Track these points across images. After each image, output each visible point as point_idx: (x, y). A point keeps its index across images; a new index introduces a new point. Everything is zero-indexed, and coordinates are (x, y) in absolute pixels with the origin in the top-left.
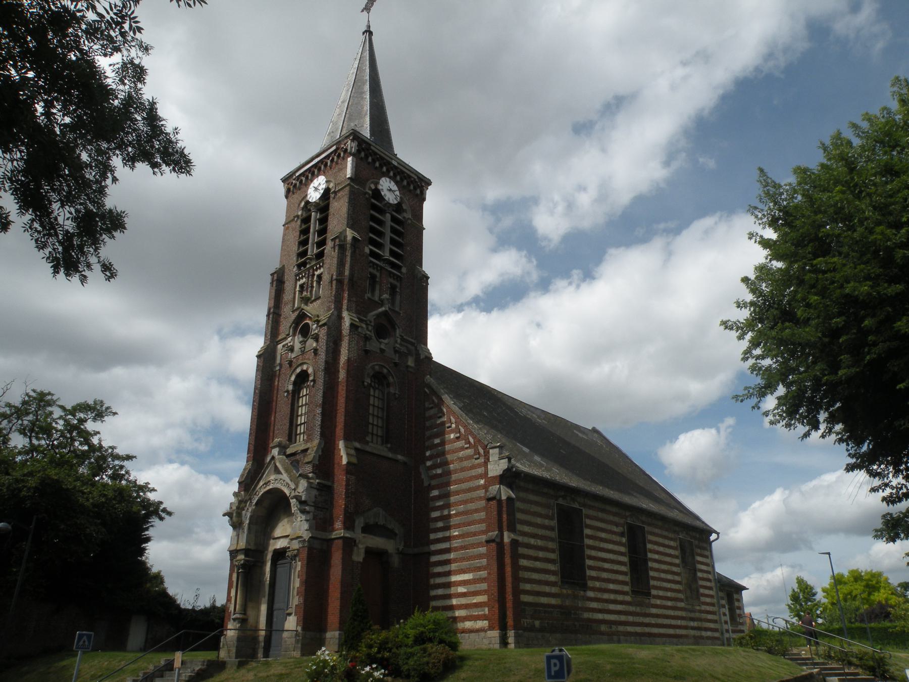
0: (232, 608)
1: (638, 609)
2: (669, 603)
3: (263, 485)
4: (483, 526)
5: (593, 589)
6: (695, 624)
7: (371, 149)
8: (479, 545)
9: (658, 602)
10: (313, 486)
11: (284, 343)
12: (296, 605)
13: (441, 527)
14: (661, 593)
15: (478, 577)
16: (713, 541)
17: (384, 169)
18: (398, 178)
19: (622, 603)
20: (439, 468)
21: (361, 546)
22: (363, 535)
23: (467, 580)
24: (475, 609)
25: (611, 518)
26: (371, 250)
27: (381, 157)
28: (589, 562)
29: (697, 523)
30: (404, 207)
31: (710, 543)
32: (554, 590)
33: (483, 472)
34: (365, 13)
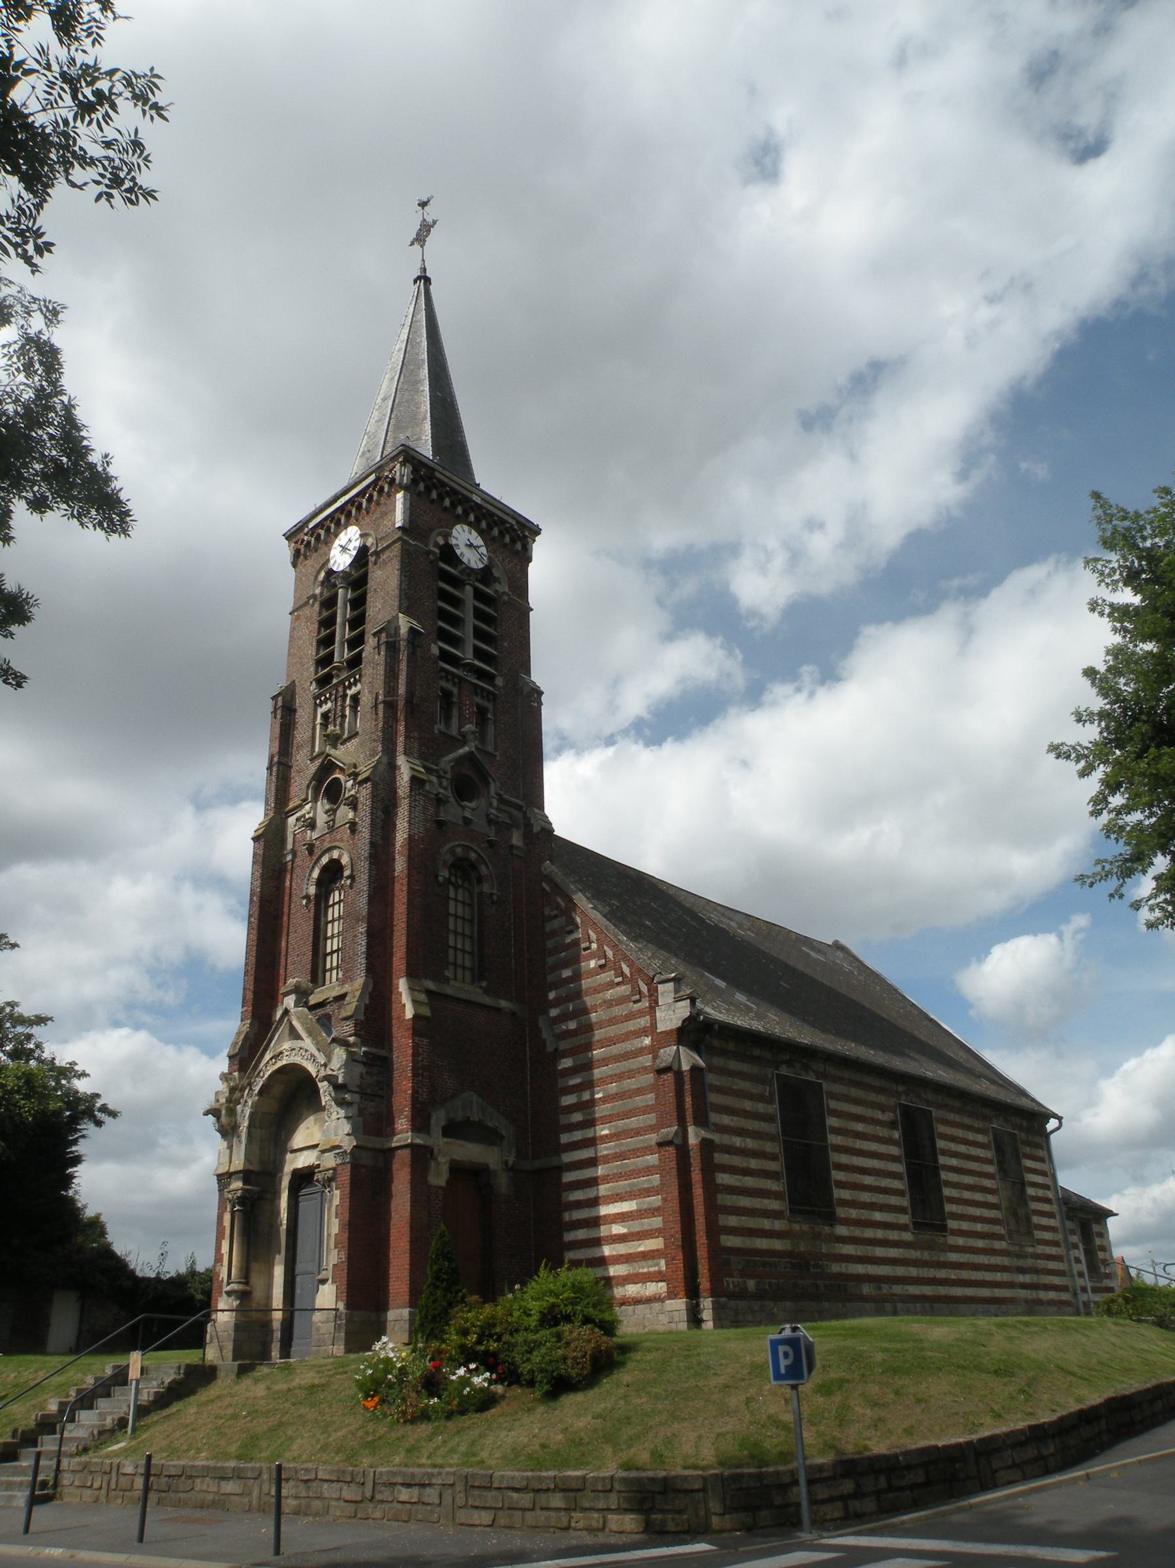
0: (224, 1274)
1: (926, 1256)
2: (980, 1243)
3: (271, 1059)
5: (846, 1222)
8: (646, 1150)
9: (961, 1241)
10: (356, 1057)
14: (965, 1226)
16: (1052, 1132)
17: (460, 510)
18: (484, 524)
21: (441, 1159)
22: (445, 1140)
23: (627, 1212)
25: (872, 1097)
26: (441, 650)
27: (452, 489)
28: (836, 1175)
29: (1024, 1102)
31: (1046, 1136)
32: (778, 1225)
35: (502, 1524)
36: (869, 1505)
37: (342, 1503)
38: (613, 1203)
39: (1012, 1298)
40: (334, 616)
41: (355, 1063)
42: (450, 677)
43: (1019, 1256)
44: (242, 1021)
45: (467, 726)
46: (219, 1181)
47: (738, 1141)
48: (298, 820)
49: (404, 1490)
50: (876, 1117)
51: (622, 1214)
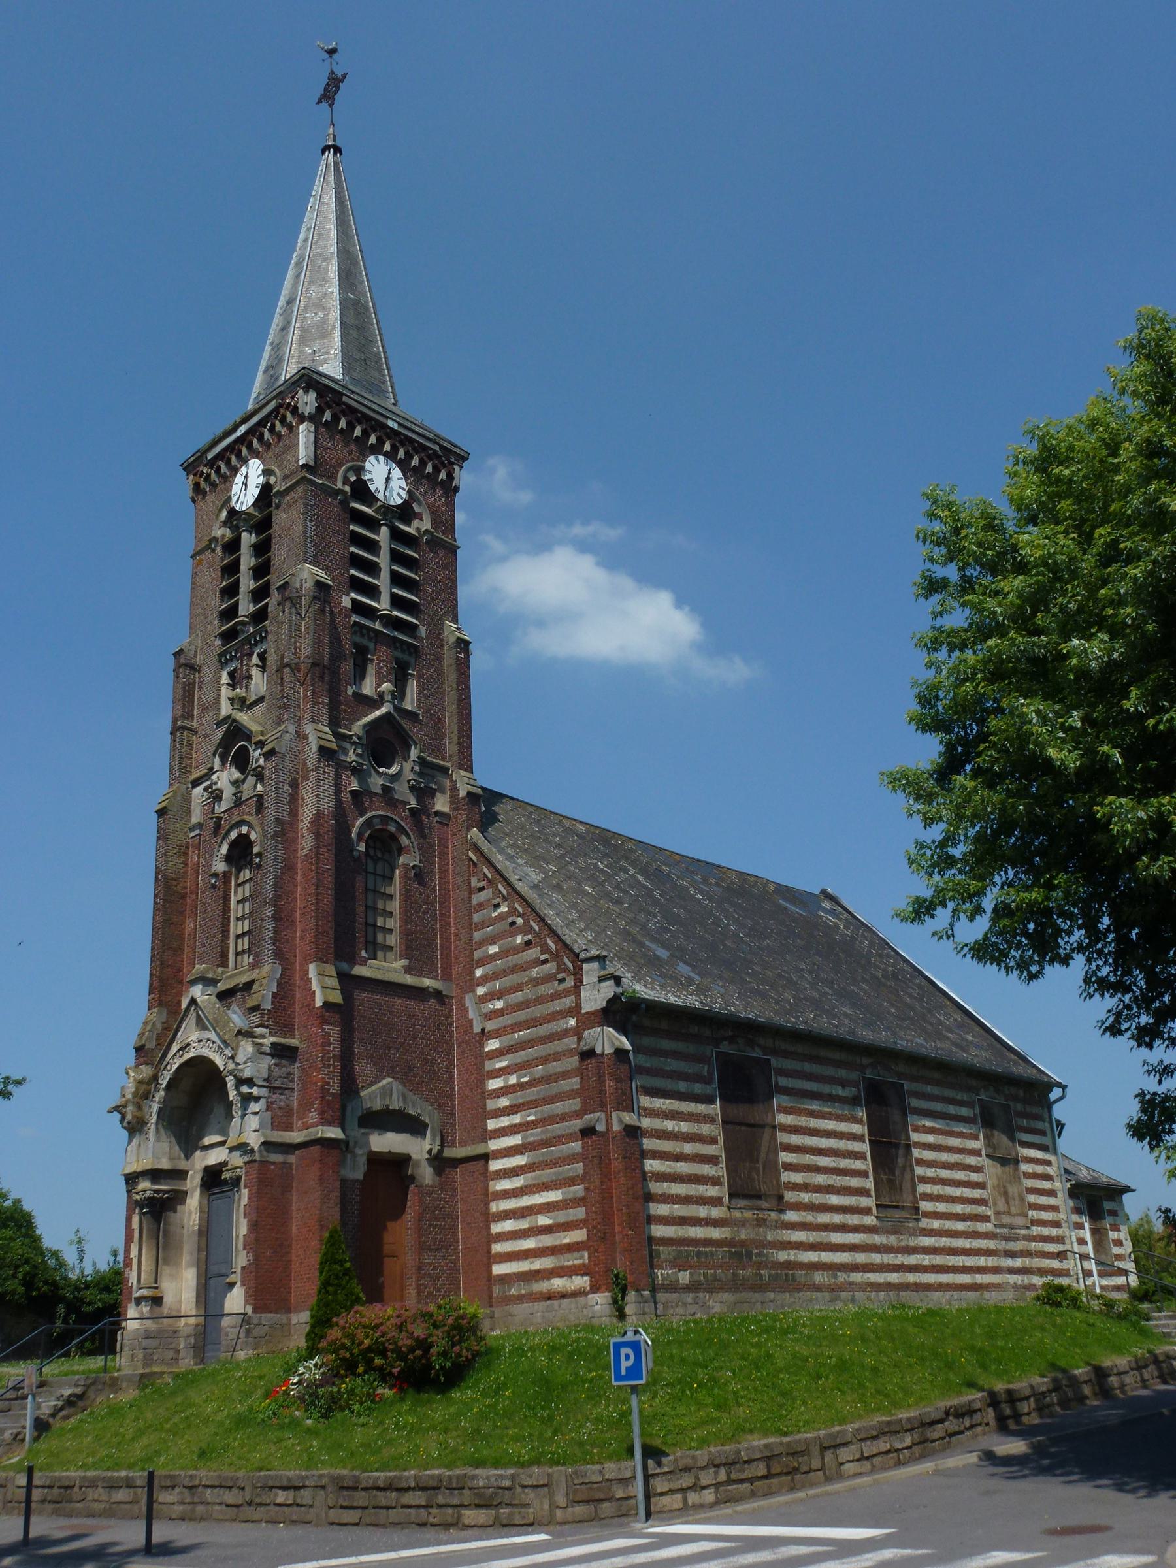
0: (133, 1280)
1: (892, 1240)
2: (960, 1226)
3: (178, 1051)
4: (575, 1104)
5: (798, 1207)
6: (1018, 1263)
7: (345, 403)
8: (570, 1138)
9: (936, 1224)
10: (264, 1049)
11: (206, 784)
12: (243, 1268)
13: (506, 1108)
14: (941, 1207)
15: (571, 1196)
16: (1055, 1102)
17: (373, 440)
19: (856, 1229)
20: (499, 999)
21: (359, 1151)
22: (363, 1131)
23: (553, 1202)
24: (568, 1256)
25: (830, 1071)
26: (353, 600)
27: (364, 414)
28: (786, 1157)
29: (1020, 1070)
30: (416, 508)
31: (1049, 1106)
32: (716, 1212)
33: (573, 1005)
34: (339, 73)
35: (368, 1522)
36: (709, 1496)
37: (224, 1507)
38: (539, 1192)
39: (999, 1284)
40: (237, 561)
41: (263, 1056)
42: (364, 631)
43: (1008, 1239)
44: (149, 1009)
45: (385, 685)
46: (127, 1183)
47: (670, 1125)
48: (205, 789)
49: (280, 1492)
50: (834, 1092)
51: (548, 1204)
